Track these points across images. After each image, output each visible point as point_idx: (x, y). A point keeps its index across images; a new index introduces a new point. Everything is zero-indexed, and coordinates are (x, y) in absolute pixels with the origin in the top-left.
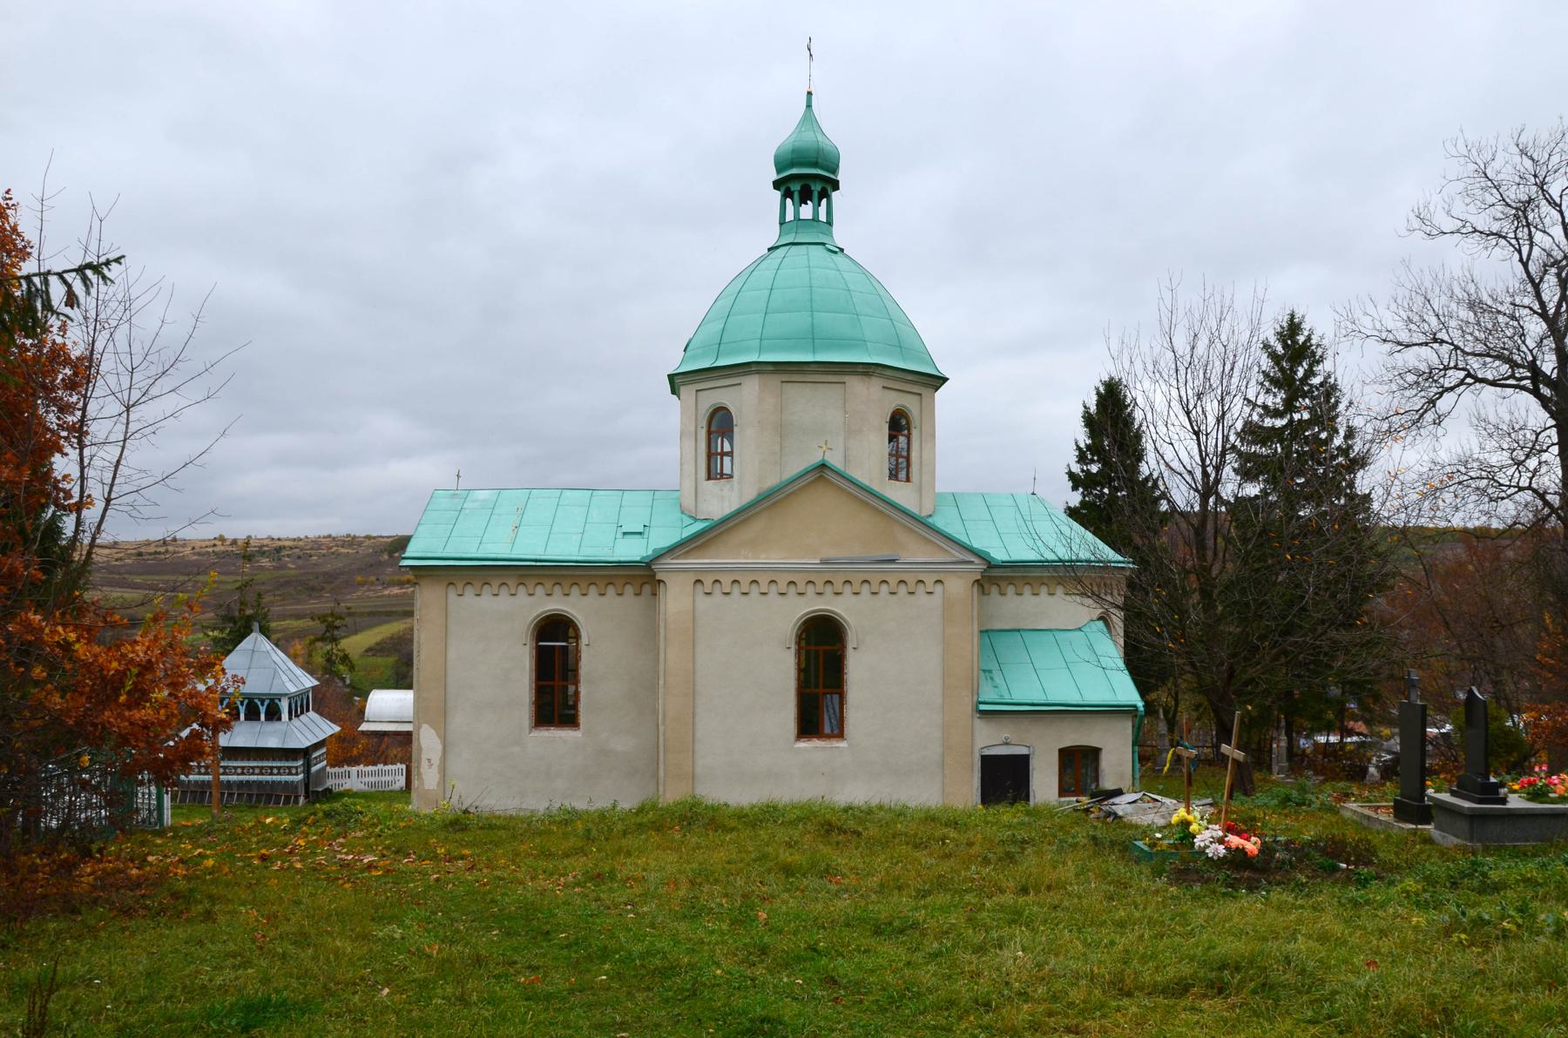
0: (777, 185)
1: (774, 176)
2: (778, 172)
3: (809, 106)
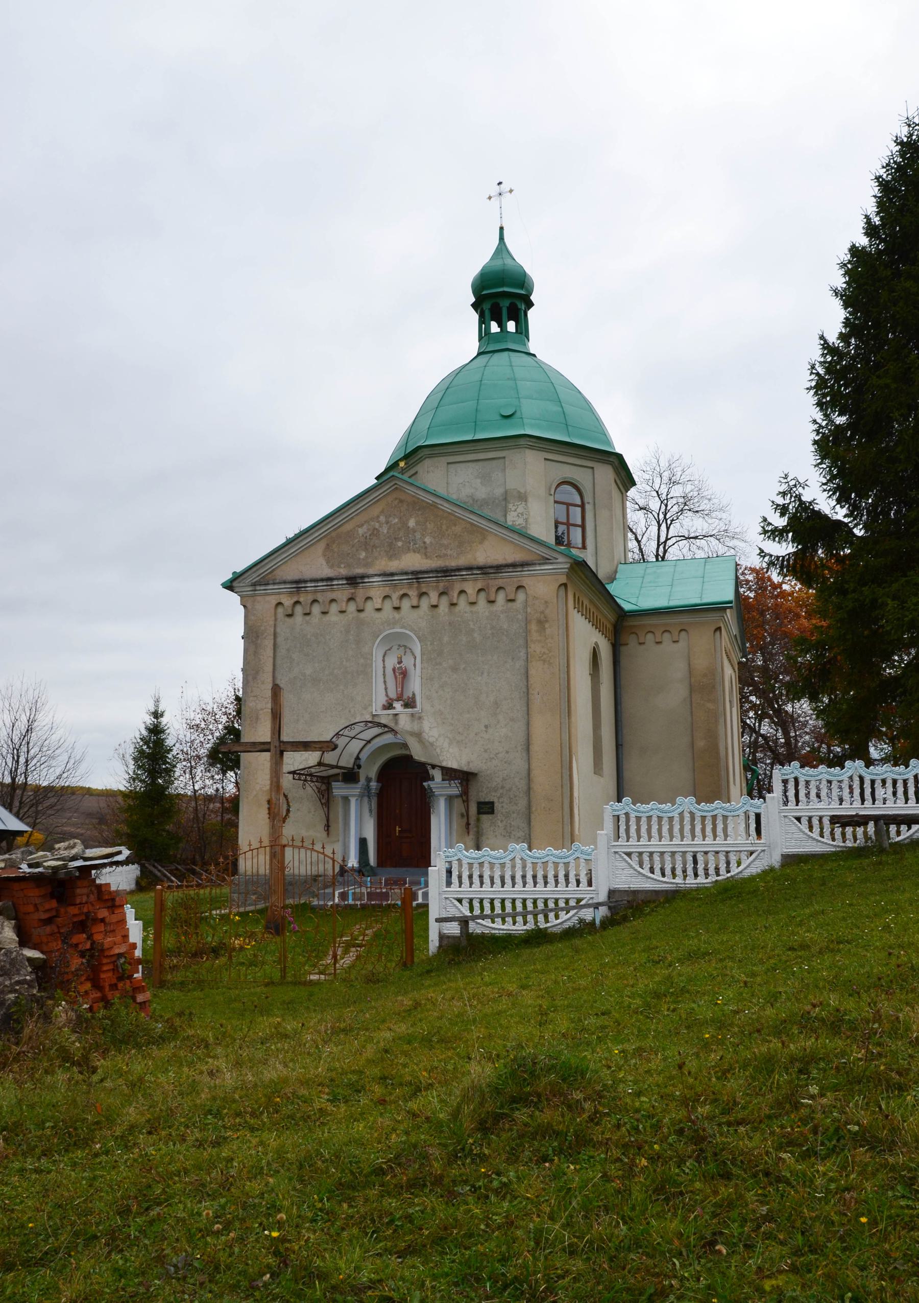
3: (501, 238)
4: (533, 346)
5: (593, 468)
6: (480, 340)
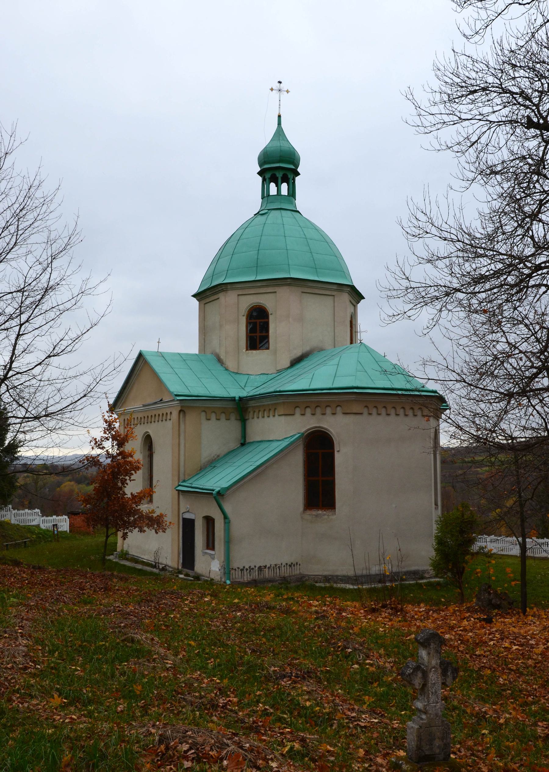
0: (260, 173)
1: (259, 169)
2: (260, 166)
3: (279, 123)
4: (300, 202)
5: (334, 296)
6: (262, 199)
